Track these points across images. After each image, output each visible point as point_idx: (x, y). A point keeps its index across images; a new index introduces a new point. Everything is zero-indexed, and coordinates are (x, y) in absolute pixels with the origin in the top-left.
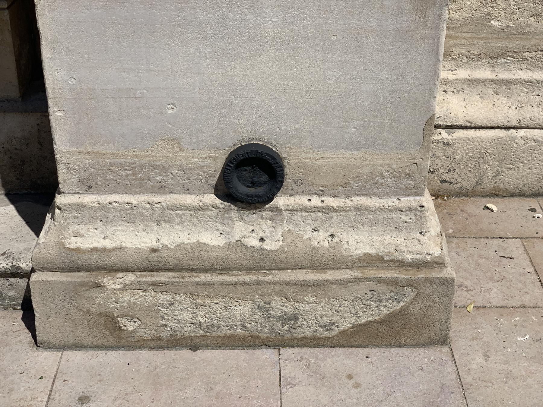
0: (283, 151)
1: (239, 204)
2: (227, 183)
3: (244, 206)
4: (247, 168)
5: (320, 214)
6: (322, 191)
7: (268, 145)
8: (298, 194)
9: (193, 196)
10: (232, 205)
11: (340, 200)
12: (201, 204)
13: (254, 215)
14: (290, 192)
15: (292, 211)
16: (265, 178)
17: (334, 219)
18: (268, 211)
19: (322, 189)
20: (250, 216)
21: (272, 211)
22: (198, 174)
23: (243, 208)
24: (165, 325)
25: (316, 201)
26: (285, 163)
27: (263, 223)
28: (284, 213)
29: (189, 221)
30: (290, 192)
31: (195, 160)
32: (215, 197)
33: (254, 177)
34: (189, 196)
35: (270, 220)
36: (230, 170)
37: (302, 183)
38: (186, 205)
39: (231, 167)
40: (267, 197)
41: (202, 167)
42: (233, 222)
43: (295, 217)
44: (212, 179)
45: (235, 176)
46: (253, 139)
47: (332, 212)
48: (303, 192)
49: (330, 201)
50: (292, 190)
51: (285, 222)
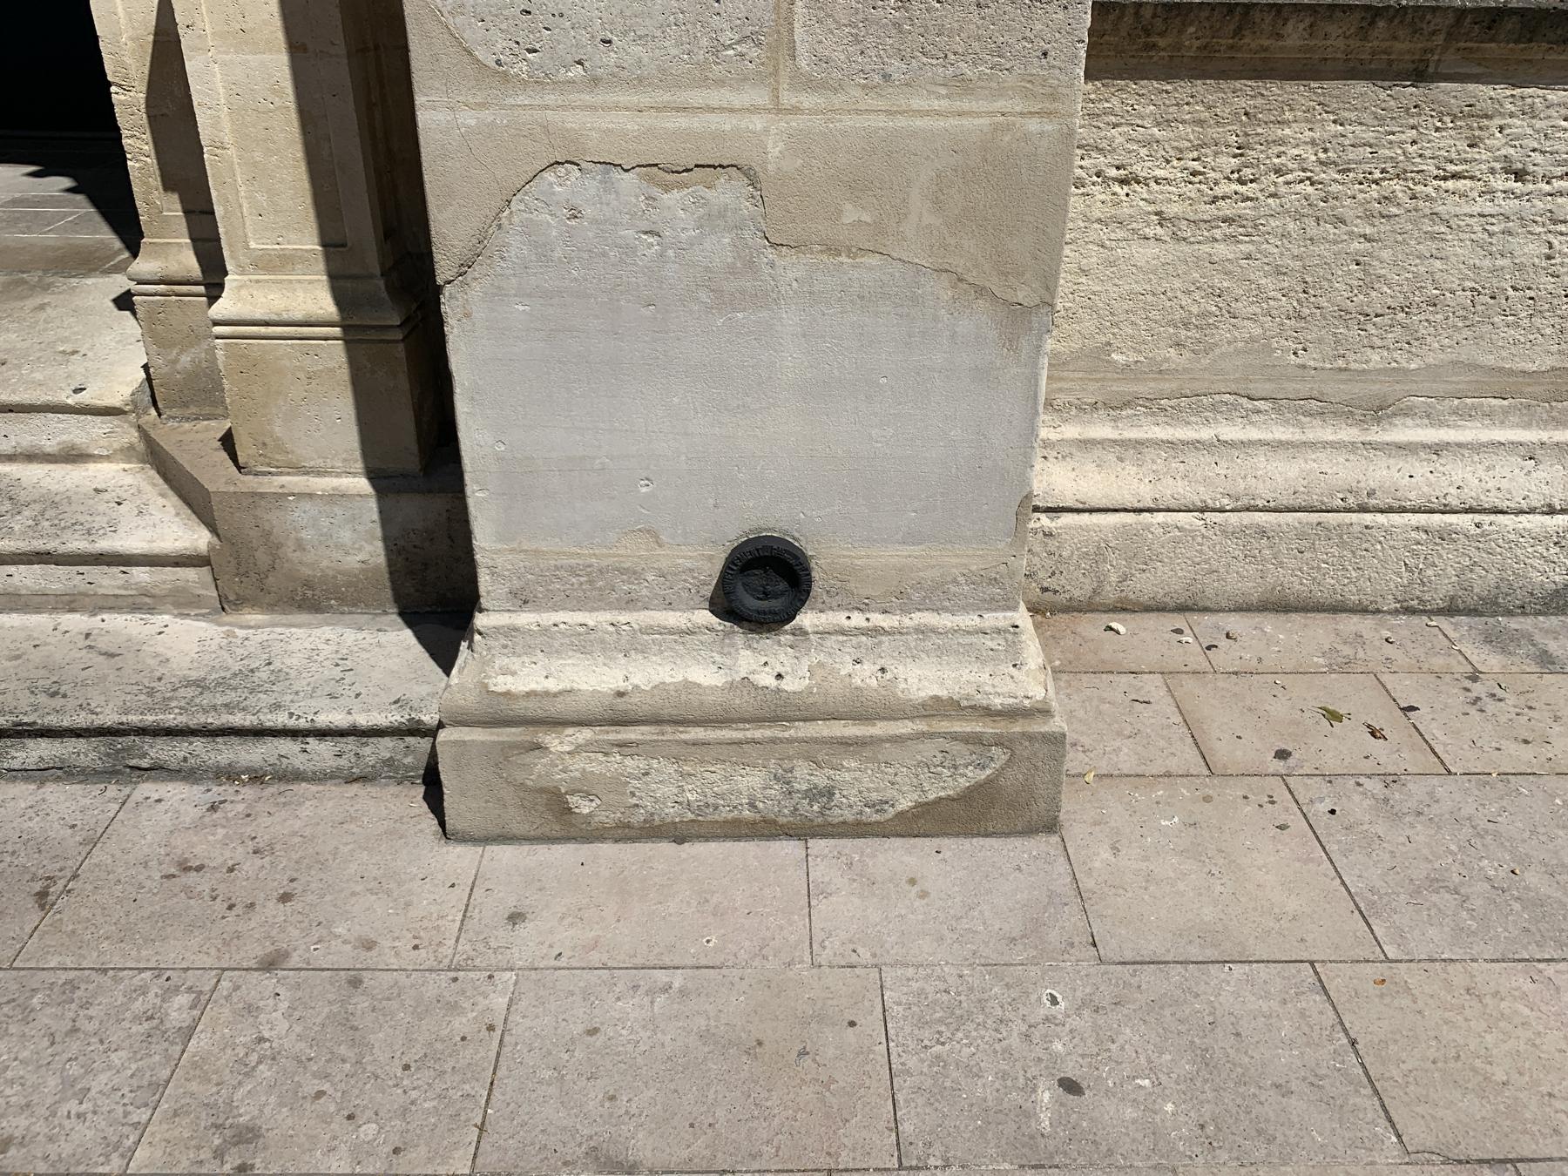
1: (746, 624)
8: (831, 609)
16: (783, 585)
23: (752, 631)
26: (813, 565)
27: (781, 651)
41: (691, 570)
49: (878, 619)
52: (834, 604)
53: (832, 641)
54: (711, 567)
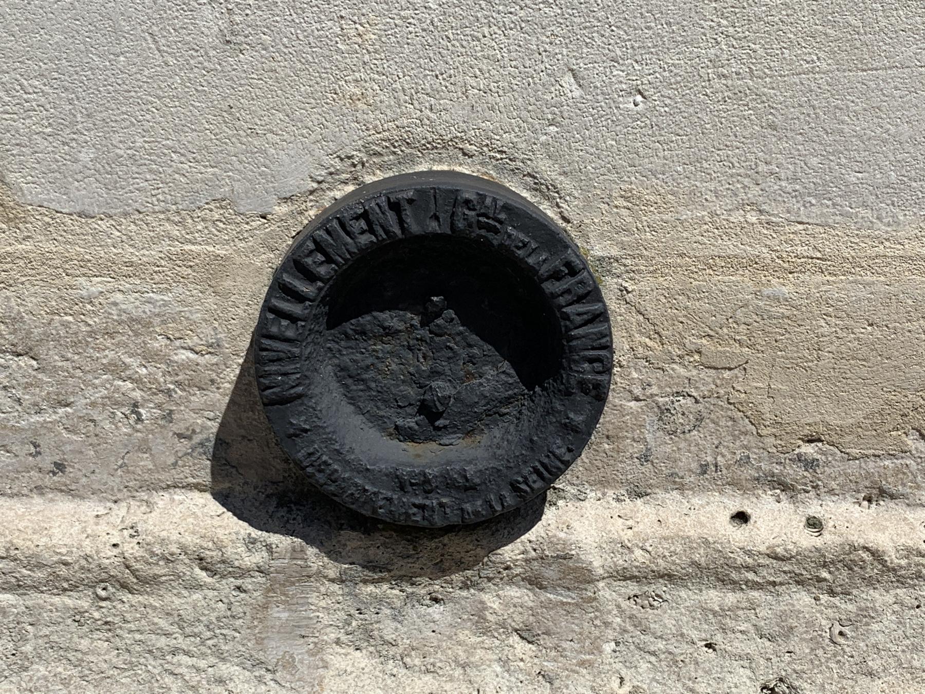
0: (593, 221)
1: (352, 539)
2: (284, 401)
3: (379, 555)
4: (391, 319)
5: (802, 599)
6: (810, 464)
7: (514, 186)
8: (675, 482)
9: (90, 508)
10: (311, 551)
11: (910, 515)
12: (131, 549)
13: (436, 611)
14: (633, 470)
15: (651, 578)
16: (495, 376)
17: (881, 630)
18: (511, 581)
19: (809, 450)
20: (412, 614)
21: (535, 582)
22: (117, 369)
23: (377, 569)
24: (859, 172)
25: (777, 523)
26: (609, 288)
27: (484, 651)
28: (606, 593)
29: (62, 651)
30: (633, 470)
31: (95, 286)
32: (215, 507)
33: (435, 373)
34: (65, 506)
35: (526, 634)
36: (293, 319)
37: (700, 419)
38: (49, 558)
39: (299, 298)
40: (514, 487)
41: (139, 325)
42: (318, 650)
43: (665, 619)
44: (197, 399)
45: (327, 370)
46: (428, 147)
47: (870, 582)
48: (704, 468)
49: (852, 521)
50: (645, 458)
51: (609, 647)
52: (687, 462)
53: (681, 611)
54: (214, 323)
